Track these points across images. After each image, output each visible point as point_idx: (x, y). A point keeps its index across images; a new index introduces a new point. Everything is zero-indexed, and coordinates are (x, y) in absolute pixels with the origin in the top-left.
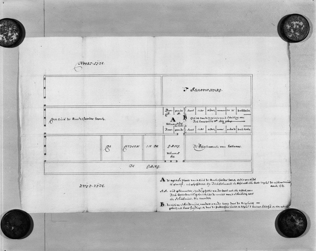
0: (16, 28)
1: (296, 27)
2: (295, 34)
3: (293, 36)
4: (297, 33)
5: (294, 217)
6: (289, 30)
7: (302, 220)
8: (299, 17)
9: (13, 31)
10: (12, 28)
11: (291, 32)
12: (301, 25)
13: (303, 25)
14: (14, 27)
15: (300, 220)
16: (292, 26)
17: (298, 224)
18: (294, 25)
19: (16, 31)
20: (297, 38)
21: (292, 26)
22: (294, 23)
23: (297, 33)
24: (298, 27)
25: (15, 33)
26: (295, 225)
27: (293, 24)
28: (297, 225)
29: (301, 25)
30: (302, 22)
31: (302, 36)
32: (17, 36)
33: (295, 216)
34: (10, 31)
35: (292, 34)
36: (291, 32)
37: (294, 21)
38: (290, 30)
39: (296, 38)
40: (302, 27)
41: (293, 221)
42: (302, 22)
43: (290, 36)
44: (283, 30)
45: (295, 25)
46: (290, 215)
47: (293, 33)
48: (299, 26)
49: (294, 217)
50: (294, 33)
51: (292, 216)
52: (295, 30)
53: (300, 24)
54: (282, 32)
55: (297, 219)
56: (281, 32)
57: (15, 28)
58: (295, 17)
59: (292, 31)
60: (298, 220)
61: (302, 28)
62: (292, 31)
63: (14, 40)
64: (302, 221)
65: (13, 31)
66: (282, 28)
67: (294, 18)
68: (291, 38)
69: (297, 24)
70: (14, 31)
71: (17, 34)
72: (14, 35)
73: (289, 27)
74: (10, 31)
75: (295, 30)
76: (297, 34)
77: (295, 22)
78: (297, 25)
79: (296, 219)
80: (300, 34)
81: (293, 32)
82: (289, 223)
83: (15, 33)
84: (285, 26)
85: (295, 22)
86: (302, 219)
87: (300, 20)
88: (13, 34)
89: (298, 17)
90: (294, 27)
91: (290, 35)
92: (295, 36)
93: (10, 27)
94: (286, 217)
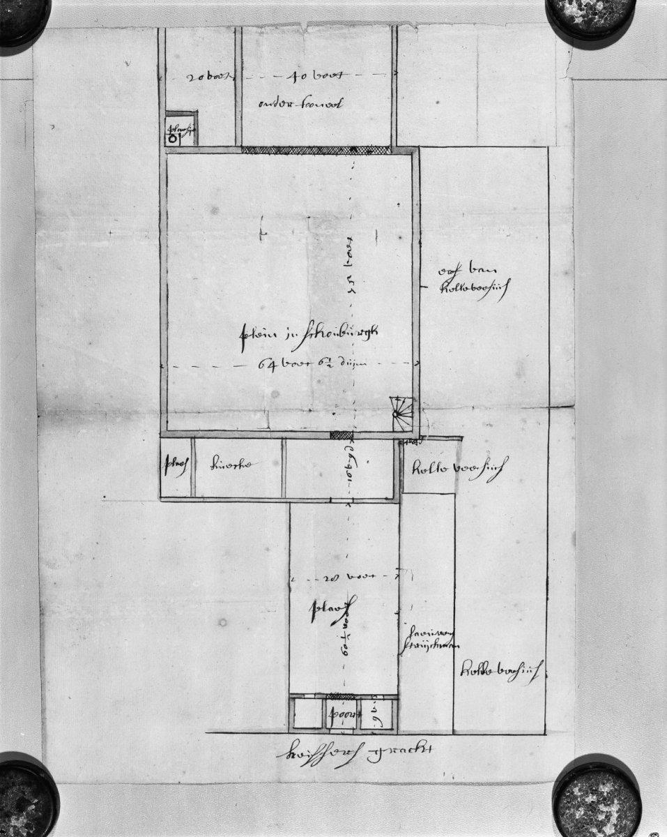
0: (596, 23)
1: (602, 812)
2: (579, 806)
3: (576, 797)
4: (582, 811)
5: (33, 807)
6: (596, 790)
7: (28, 833)
8: (630, 825)
9: (591, 12)
10: (600, 12)
11: (587, 793)
12: (604, 829)
13: (604, 832)
14: (602, 17)
15: (27, 826)
16: (607, 801)
17: (13, 822)
18: (609, 805)
19: (588, 22)
20: (568, 811)
21: (605, 799)
22: (614, 808)
23: (582, 811)
24: (601, 817)
25: (583, 16)
26: (8, 816)
27: (613, 803)
28: (10, 821)
29: (604, 829)
30: (613, 831)
31: (569, 826)
32: (572, 18)
33: (36, 810)
34: (595, 4)
35: (581, 796)
36: (586, 794)
37: (619, 809)
38: (594, 792)
39: (569, 808)
40: (599, 832)
41: (21, 807)
42: (613, 831)
43: (576, 791)
44: (599, 772)
45: (607, 809)
46: (36, 795)
47: (584, 800)
48: (601, 821)
49: (33, 807)
50: (583, 804)
51: (36, 801)
52: (592, 807)
53: (609, 825)
54: (591, 767)
55: (27, 818)
56: (591, 764)
57: (599, 21)
58: (631, 815)
59: (590, 799)
60: (25, 821)
61: (595, 830)
62: (590, 799)
63: (564, 6)
64: (25, 834)
65: (591, 12)
66: (602, 767)
67: (630, 809)
68: (569, 792)
69: (608, 817)
70: (590, 16)
71: (578, 20)
72: (579, 12)
73: (606, 789)
74: (595, 4)
75: (592, 807)
76: (580, 813)
77: (617, 812)
78: (606, 817)
79: (27, 813)
80: (577, 820)
81: (587, 800)
82: (12, 795)
83: (581, 16)
84: (608, 780)
85: (617, 812)
86: (31, 832)
87: (621, 826)
88: (581, 10)
89: (632, 821)
90: (602, 807)
91: (580, 790)
92: (574, 806)
93: (604, 8)
94: (29, 784)
